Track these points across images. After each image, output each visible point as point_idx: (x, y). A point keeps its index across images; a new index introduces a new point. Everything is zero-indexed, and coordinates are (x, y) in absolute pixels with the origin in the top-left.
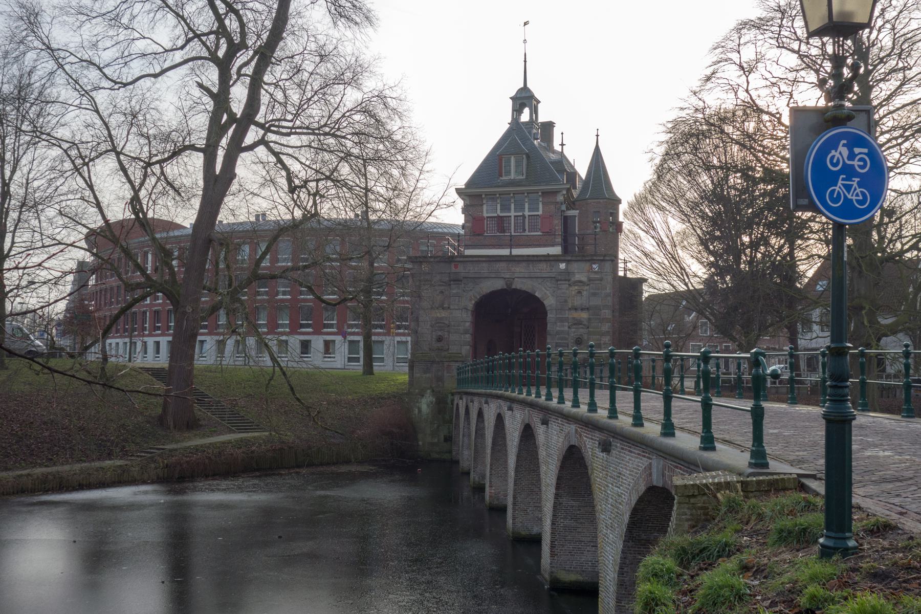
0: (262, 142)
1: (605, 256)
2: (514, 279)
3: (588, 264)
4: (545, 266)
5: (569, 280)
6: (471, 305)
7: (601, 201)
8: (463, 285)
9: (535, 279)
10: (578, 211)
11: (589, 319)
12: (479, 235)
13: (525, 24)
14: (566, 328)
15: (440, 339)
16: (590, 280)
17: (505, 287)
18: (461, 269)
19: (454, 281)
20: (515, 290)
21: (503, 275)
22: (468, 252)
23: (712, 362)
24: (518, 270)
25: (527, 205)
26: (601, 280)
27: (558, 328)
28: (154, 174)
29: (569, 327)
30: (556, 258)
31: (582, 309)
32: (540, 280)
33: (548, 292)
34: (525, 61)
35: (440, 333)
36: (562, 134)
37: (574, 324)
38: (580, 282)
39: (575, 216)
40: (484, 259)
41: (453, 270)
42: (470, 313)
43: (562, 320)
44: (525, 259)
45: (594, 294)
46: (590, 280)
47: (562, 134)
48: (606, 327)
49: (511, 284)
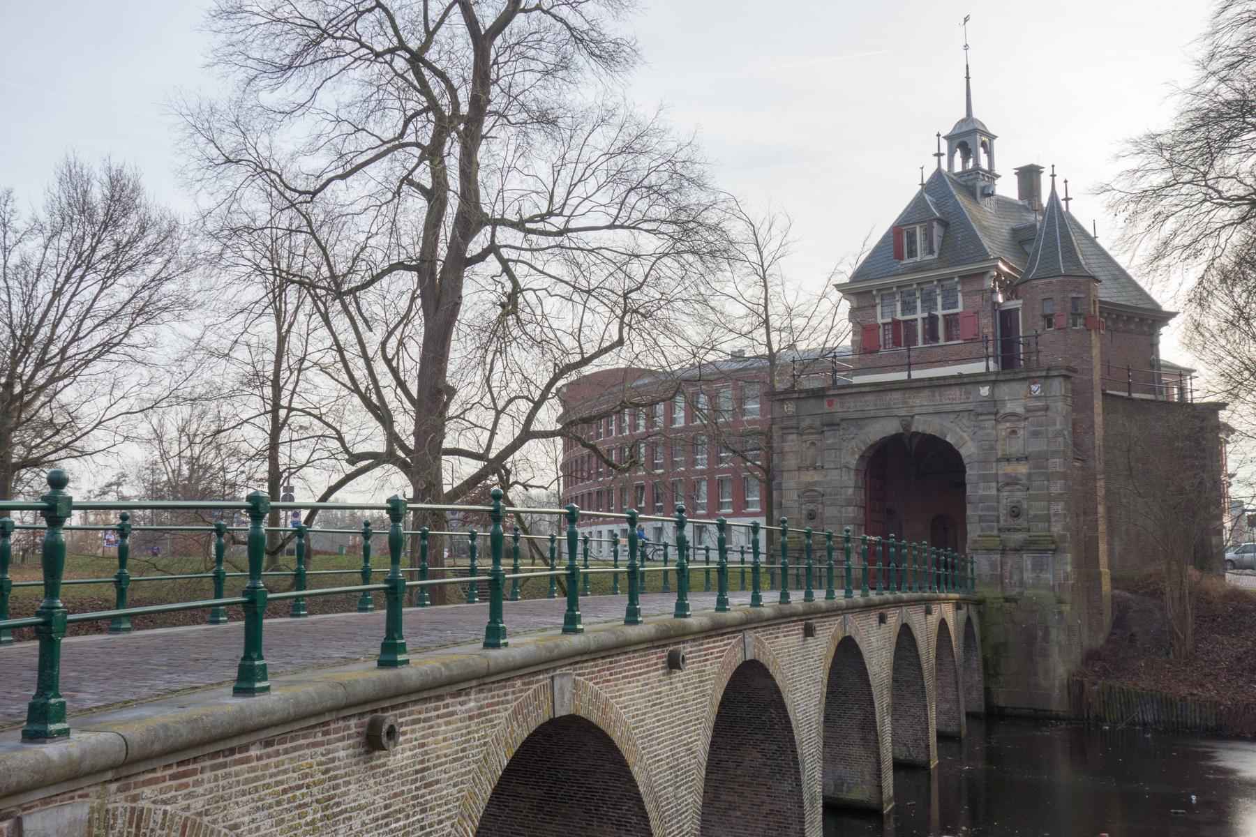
0: (493, 249)
1: (1049, 369)
2: (912, 417)
3: (1025, 385)
4: (958, 393)
5: (996, 414)
6: (853, 461)
7: (1054, 280)
8: (841, 432)
9: (943, 415)
10: (1021, 301)
11: (1029, 475)
12: (871, 352)
13: (966, 19)
14: (994, 492)
15: (812, 516)
16: (1028, 410)
17: (902, 431)
18: (837, 407)
19: (828, 425)
20: (916, 434)
21: (896, 412)
22: (857, 380)
23: (556, 542)
24: (918, 402)
25: (939, 300)
26: (1047, 409)
27: (981, 492)
28: (376, 303)
29: (998, 490)
30: (972, 379)
31: (1018, 460)
32: (952, 416)
33: (965, 435)
34: (968, 78)
35: (812, 506)
36: (1066, 182)
37: (1007, 484)
38: (1014, 414)
39: (1017, 310)
40: (867, 389)
41: (826, 409)
42: (852, 473)
43: (985, 479)
44: (926, 384)
45: (1035, 434)
46: (1028, 410)
47: (1066, 182)
48: (1057, 487)
49: (910, 426)
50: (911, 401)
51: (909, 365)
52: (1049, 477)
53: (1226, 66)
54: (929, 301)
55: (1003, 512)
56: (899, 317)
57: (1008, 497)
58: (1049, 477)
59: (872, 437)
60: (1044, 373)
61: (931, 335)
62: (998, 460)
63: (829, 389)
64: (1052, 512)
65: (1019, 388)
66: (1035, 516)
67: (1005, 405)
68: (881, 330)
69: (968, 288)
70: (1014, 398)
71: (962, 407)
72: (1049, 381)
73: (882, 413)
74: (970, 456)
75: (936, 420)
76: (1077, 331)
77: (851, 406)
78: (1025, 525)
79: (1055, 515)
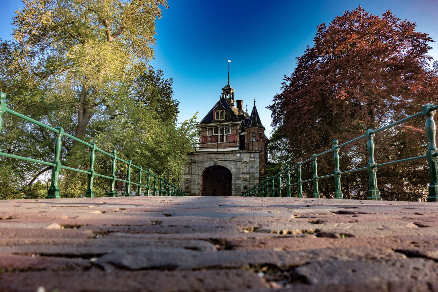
3: (249, 154)
6: (201, 173)
7: (256, 128)
9: (227, 161)
11: (250, 178)
12: (205, 143)
14: (240, 182)
16: (250, 161)
18: (196, 157)
21: (214, 160)
22: (200, 151)
24: (220, 157)
26: (255, 161)
27: (236, 182)
31: (247, 174)
32: (229, 162)
35: (187, 185)
37: (244, 180)
40: (206, 153)
44: (222, 152)
45: (252, 167)
46: (250, 161)
50: (218, 157)
51: (217, 147)
52: (255, 179)
53: (36, 197)
54: (222, 132)
55: (242, 188)
57: (243, 184)
58: (255, 179)
59: (206, 166)
60: (255, 152)
61: (222, 140)
62: (242, 174)
63: (195, 152)
65: (248, 155)
69: (233, 128)
70: (246, 157)
71: (232, 159)
72: (255, 154)
73: (209, 160)
74: (233, 172)
75: (224, 162)
76: (261, 142)
77: (201, 157)
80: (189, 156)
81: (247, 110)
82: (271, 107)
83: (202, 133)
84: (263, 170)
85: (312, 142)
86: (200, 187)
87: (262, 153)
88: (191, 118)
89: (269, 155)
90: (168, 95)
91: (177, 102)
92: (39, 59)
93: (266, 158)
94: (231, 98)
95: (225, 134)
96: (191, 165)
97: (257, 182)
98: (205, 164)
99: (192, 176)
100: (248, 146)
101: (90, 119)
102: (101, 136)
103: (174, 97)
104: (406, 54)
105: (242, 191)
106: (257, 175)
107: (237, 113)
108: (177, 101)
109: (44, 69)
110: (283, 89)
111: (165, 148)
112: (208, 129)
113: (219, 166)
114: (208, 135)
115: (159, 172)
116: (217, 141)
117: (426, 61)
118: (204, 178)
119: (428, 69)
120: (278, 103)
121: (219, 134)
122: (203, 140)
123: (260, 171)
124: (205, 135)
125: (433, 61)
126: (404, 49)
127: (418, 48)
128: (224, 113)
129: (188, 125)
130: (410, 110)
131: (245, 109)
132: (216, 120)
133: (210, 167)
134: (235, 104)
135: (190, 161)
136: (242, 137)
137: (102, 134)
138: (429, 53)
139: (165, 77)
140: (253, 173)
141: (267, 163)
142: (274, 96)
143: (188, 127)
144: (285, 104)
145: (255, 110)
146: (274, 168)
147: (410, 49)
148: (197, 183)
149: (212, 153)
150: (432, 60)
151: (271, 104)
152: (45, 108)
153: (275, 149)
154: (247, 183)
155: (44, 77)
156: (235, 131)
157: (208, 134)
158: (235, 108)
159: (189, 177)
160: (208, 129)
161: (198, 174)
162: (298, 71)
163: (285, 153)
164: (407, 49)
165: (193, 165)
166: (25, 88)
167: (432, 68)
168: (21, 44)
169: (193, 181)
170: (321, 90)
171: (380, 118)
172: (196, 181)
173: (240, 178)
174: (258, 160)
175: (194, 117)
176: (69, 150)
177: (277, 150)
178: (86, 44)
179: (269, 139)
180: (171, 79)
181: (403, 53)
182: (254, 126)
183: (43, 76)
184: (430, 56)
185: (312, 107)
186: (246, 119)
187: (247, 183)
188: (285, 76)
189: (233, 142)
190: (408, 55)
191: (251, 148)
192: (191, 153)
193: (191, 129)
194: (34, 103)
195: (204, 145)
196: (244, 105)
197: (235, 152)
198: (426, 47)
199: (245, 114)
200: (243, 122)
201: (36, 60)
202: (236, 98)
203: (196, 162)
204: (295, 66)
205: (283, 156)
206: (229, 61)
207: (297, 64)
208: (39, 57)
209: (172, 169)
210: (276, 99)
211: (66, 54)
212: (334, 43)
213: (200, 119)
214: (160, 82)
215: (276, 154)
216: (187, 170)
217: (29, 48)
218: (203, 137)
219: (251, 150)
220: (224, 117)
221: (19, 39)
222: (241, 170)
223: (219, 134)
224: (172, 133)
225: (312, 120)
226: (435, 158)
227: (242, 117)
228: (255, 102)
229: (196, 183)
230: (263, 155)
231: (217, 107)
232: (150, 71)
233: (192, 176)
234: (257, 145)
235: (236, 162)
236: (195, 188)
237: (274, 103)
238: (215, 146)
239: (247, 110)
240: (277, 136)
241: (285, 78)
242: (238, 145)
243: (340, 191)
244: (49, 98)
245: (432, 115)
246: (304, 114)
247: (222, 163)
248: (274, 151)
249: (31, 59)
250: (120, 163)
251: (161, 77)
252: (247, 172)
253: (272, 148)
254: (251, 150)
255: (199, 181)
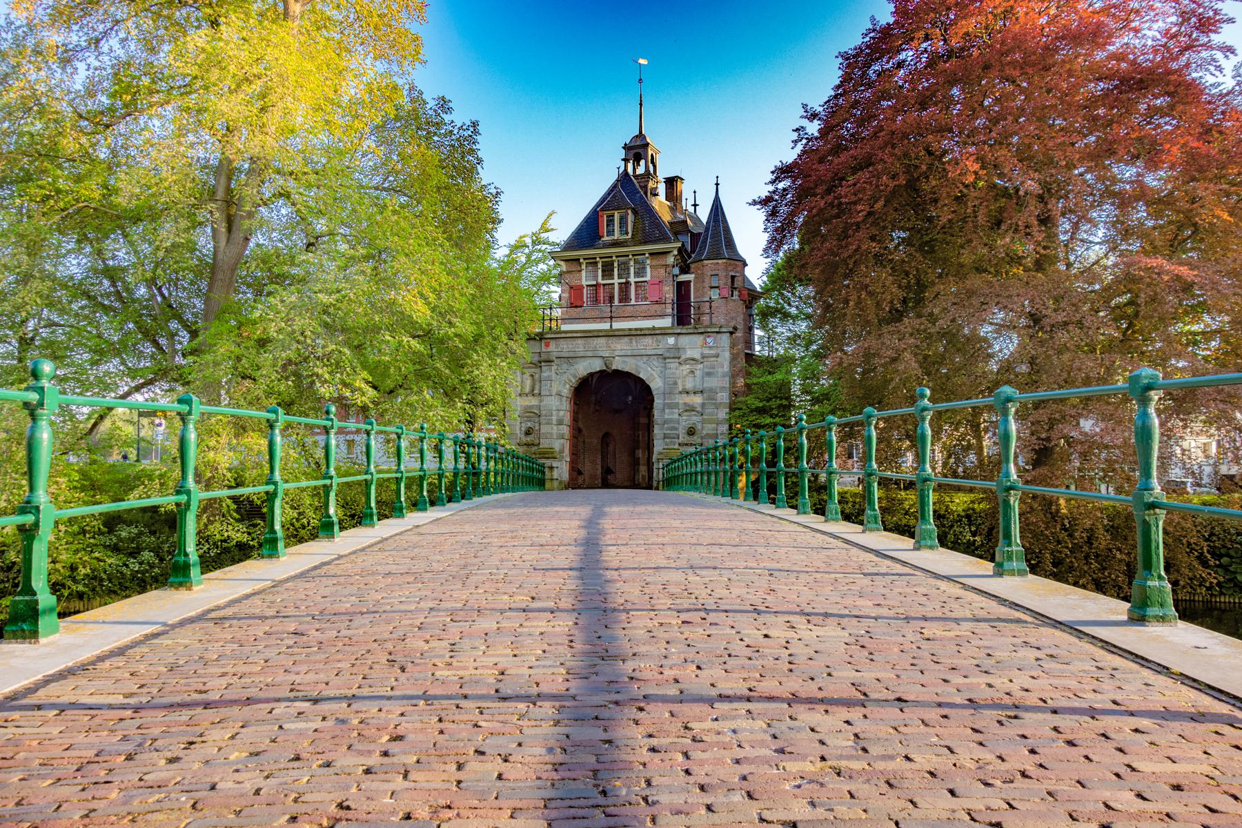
3: (701, 337)
6: (566, 391)
7: (720, 261)
11: (703, 405)
12: (576, 307)
14: (676, 416)
18: (553, 347)
22: (564, 327)
24: (619, 347)
27: (666, 417)
32: (645, 359)
35: (529, 424)
37: (686, 411)
39: (690, 281)
40: (579, 335)
44: (627, 333)
45: (709, 374)
50: (613, 346)
51: (611, 318)
52: (717, 406)
55: (682, 432)
56: (600, 280)
57: (686, 422)
58: (717, 406)
60: (717, 330)
61: (625, 298)
62: (680, 392)
63: (547, 333)
64: (719, 432)
66: (707, 434)
67: (685, 352)
68: (585, 290)
70: (692, 346)
72: (719, 336)
73: (590, 354)
75: (631, 361)
76: (734, 301)
77: (565, 347)
78: (699, 441)
79: (722, 434)
80: (532, 342)
81: (695, 205)
82: (764, 202)
83: (568, 278)
84: (741, 382)
85: (878, 304)
86: (565, 430)
87: (739, 334)
88: (536, 228)
89: (758, 333)
90: (469, 172)
91: (494, 191)
92: (88, 70)
93: (749, 343)
94: (650, 174)
95: (632, 279)
96: (538, 370)
97: (723, 414)
98: (576, 366)
99: (541, 401)
100: (700, 314)
101: (247, 245)
102: (282, 301)
103: (486, 175)
104: (1159, 37)
105: (681, 440)
106: (724, 397)
107: (666, 217)
108: (492, 186)
109: (104, 99)
110: (799, 147)
111: (465, 328)
112: (584, 267)
113: (617, 372)
114: (584, 283)
115: (450, 394)
116: (611, 299)
117: (1214, 60)
118: (575, 403)
119: (1219, 85)
120: (784, 190)
121: (616, 281)
122: (570, 297)
123: (733, 384)
124: (575, 283)
125: (1234, 60)
126: (1153, 21)
127: (1194, 20)
128: (630, 218)
129: (527, 251)
130: (1159, 203)
131: (691, 202)
132: (606, 238)
133: (591, 375)
134: (662, 189)
135: (536, 358)
136: (682, 290)
137: (284, 293)
138: (1224, 35)
139: (459, 117)
140: (712, 391)
141: (750, 358)
142: (773, 169)
143: (529, 256)
144: (803, 194)
145: (717, 209)
146: (770, 377)
147: (1171, 23)
148: (557, 420)
149: (596, 334)
150: (1231, 56)
151: (764, 191)
152: (119, 217)
153: (775, 317)
154: (695, 419)
155: (107, 126)
156: (662, 271)
157: (584, 279)
158: (660, 203)
159: (533, 401)
160: (584, 267)
161: (559, 394)
162: (841, 95)
163: (803, 326)
164: (1160, 24)
165: (544, 368)
166: (52, 154)
167: (1228, 83)
168: (31, 26)
169: (544, 413)
170: (906, 155)
171: (1076, 227)
172: (554, 413)
173: (676, 406)
174: (727, 355)
175: (545, 228)
176: (194, 334)
177: (781, 319)
178: (223, 28)
179: (759, 290)
180: (475, 124)
181: (1149, 33)
182: (716, 255)
183: (103, 121)
184: (1228, 44)
185: (881, 203)
186: (692, 233)
187: (695, 419)
188: (805, 106)
189: (657, 302)
190: (1164, 40)
191: (706, 319)
192: (537, 334)
193: (537, 262)
194: (85, 201)
195: (574, 312)
196: (686, 190)
197: (663, 332)
198: (1218, 17)
199: (690, 216)
200: (683, 245)
201: (79, 71)
202: (663, 172)
203: (552, 361)
204: (835, 76)
205: (797, 336)
206: (643, 61)
207: (841, 73)
208: (88, 61)
209: (486, 385)
210: (777, 178)
211: (165, 56)
212: (949, 9)
213: (563, 231)
214: (443, 131)
215: (778, 330)
216: (528, 382)
217: (54, 38)
218: (571, 288)
219: (707, 327)
220: (630, 230)
221: (25, 14)
222: (680, 382)
223: (616, 281)
224: (481, 282)
225: (879, 242)
226: (1152, 512)
227: (679, 227)
228: (717, 184)
229: (554, 418)
230: (741, 340)
231: (610, 202)
232: (412, 101)
233: (541, 401)
234: (723, 310)
235: (665, 359)
236: (551, 434)
237: (771, 188)
238: (605, 315)
239: (695, 205)
240: (781, 279)
241: (806, 111)
242: (669, 311)
243: (930, 524)
244: (128, 192)
245: (1150, 400)
246: (858, 225)
247: (624, 362)
248: (774, 322)
249: (64, 69)
250: (338, 375)
251: (444, 116)
252: (695, 387)
253: (766, 314)
254: (707, 327)
255: (562, 413)
